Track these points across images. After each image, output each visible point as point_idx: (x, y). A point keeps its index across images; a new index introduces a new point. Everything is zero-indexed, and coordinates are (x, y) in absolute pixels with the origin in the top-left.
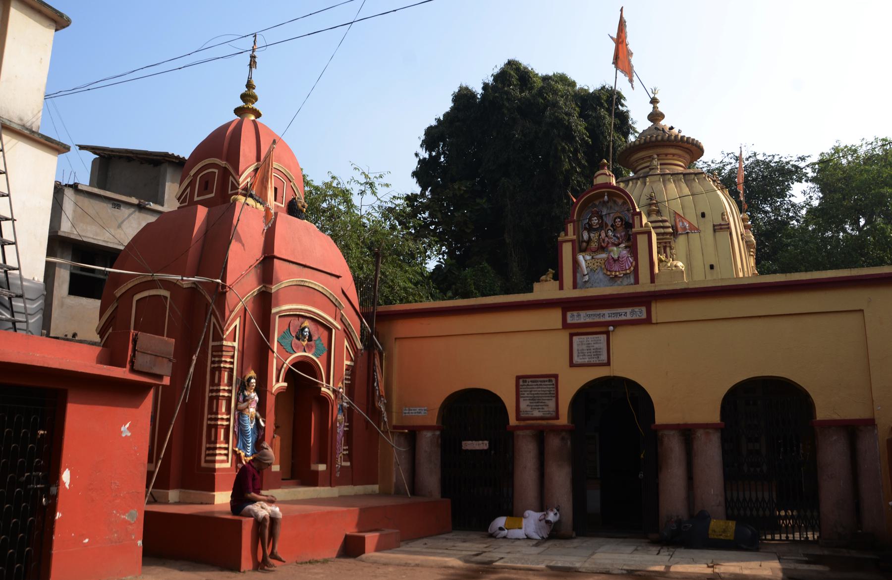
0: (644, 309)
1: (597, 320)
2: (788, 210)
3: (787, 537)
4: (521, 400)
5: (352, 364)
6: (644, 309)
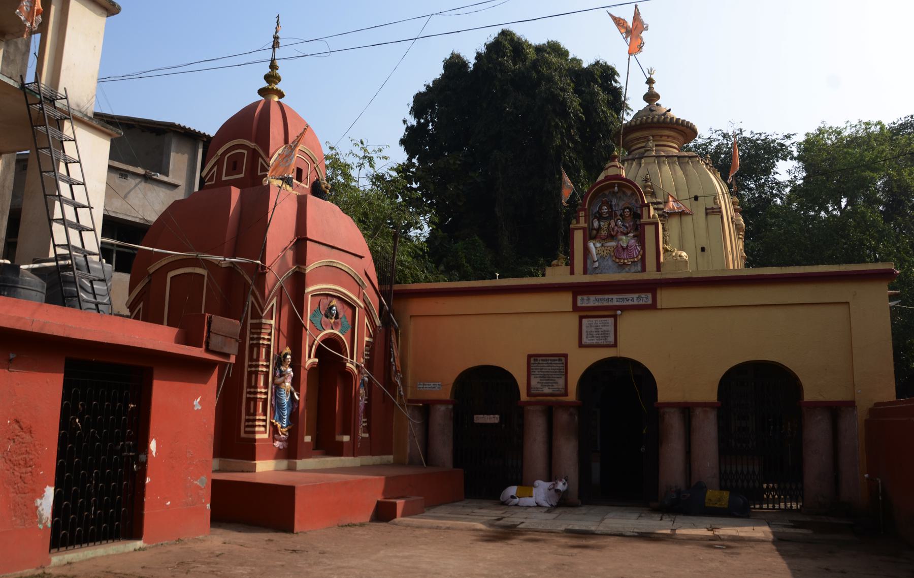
0: (650, 295)
1: (605, 304)
2: (772, 188)
3: (774, 506)
4: (532, 377)
5: (371, 340)
6: (650, 295)
